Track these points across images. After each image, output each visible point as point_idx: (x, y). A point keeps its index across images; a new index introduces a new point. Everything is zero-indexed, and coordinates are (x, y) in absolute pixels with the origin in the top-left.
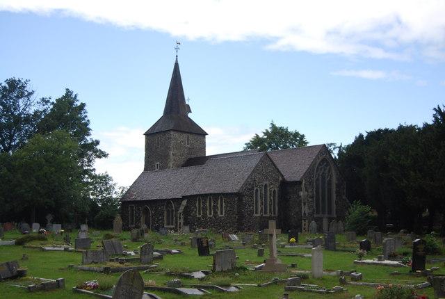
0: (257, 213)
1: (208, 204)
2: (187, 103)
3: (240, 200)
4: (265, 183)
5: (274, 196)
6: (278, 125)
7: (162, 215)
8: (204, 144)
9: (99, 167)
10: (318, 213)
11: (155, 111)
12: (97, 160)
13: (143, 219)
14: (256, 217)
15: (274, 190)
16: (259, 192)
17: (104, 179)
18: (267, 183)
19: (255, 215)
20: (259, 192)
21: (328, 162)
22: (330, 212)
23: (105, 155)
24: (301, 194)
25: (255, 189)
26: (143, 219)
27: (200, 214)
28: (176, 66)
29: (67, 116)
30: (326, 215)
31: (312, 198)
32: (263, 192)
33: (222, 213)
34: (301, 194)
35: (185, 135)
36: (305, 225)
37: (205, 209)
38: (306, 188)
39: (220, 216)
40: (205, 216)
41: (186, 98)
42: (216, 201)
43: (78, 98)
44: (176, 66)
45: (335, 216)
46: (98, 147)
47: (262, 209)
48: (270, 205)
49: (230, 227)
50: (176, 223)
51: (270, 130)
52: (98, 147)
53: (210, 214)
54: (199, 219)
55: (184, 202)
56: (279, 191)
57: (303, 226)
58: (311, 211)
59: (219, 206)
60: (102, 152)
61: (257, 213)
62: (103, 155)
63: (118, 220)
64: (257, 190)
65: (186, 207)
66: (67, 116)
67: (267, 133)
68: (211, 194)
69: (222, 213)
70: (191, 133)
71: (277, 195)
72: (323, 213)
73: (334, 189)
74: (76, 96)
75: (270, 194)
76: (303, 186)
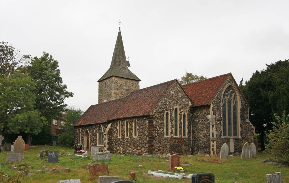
1: (125, 127)
3: (151, 122)
4: (175, 107)
7: (96, 136)
9: (70, 103)
10: (225, 135)
11: (105, 64)
14: (166, 139)
15: (184, 115)
16: (169, 115)
18: (178, 107)
19: (165, 136)
20: (169, 115)
21: (233, 89)
22: (235, 134)
23: (71, 95)
24: (209, 117)
25: (166, 112)
27: (120, 136)
28: (120, 34)
29: (45, 71)
31: (220, 120)
33: (136, 135)
34: (209, 117)
35: (124, 80)
36: (213, 146)
37: (123, 131)
38: (214, 111)
39: (134, 137)
44: (120, 34)
45: (240, 137)
47: (172, 131)
48: (180, 128)
49: (143, 147)
51: (185, 76)
54: (119, 139)
55: (109, 126)
56: (189, 115)
58: (219, 133)
59: (133, 128)
60: (67, 93)
61: (167, 134)
64: (167, 114)
65: (111, 130)
66: (45, 71)
67: (262, 72)
69: (136, 135)
70: (128, 79)
71: (186, 119)
72: (230, 134)
73: (239, 111)
74: (51, 56)
75: (181, 118)
76: (211, 110)
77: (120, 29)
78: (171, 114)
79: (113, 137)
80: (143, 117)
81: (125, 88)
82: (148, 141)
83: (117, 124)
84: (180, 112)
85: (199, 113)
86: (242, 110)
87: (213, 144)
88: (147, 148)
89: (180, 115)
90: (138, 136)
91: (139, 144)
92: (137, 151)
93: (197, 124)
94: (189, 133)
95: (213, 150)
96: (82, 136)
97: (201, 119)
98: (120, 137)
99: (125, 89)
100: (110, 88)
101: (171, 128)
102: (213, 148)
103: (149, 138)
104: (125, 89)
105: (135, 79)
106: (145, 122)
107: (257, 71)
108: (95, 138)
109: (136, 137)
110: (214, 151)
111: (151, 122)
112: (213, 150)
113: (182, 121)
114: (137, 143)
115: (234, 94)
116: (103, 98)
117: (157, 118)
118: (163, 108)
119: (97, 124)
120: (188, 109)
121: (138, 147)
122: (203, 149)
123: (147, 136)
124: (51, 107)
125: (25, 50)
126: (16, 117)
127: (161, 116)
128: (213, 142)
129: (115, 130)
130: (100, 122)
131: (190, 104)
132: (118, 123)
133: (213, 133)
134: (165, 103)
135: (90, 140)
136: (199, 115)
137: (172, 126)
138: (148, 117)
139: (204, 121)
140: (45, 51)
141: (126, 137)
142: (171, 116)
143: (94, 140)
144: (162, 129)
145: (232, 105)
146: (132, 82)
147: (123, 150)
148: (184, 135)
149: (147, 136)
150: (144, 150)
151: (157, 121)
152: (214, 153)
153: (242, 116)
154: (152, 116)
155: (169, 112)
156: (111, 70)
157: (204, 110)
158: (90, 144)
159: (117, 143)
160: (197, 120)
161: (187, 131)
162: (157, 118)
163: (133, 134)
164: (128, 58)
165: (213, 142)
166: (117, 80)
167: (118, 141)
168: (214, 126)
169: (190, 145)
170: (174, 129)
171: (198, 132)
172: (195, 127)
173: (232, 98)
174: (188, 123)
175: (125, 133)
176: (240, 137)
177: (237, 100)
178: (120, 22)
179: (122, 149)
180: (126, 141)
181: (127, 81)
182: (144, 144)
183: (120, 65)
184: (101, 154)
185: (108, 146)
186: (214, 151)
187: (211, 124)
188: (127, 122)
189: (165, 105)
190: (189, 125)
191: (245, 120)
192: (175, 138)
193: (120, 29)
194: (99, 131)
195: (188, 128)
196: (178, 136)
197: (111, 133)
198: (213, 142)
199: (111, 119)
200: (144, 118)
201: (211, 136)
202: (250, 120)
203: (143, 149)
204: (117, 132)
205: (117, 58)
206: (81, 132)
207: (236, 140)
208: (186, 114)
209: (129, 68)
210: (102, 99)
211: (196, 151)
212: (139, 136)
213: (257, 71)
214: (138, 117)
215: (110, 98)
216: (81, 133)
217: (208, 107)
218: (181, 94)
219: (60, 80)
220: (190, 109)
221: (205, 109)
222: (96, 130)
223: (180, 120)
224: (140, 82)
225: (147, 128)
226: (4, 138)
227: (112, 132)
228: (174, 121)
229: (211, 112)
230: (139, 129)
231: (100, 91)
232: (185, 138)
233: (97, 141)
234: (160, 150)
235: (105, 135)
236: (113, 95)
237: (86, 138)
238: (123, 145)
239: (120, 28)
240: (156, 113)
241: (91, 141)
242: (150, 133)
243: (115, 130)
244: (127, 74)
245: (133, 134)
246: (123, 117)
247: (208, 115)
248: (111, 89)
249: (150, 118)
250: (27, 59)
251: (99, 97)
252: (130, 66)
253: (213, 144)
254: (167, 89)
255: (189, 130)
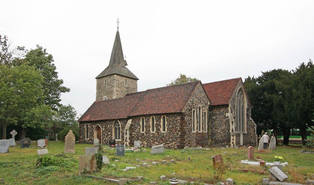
0: (194, 130)
2: (125, 59)
3: (182, 119)
5: (205, 116)
6: (183, 74)
8: (136, 85)
9: (65, 99)
11: (103, 63)
12: (62, 93)
13: (95, 134)
14: (193, 134)
15: (205, 112)
16: (195, 113)
17: (69, 109)
18: (201, 105)
19: (193, 132)
20: (195, 113)
23: (68, 90)
24: (228, 115)
26: (95, 134)
27: (143, 130)
29: (39, 60)
30: (242, 132)
32: (198, 113)
33: (164, 130)
34: (228, 115)
36: (233, 140)
39: (163, 132)
40: (148, 132)
41: (124, 56)
42: (158, 120)
43: (46, 52)
46: (62, 85)
47: (197, 127)
48: (203, 124)
50: (123, 137)
52: (62, 85)
53: (153, 130)
54: (143, 134)
55: (130, 122)
56: (208, 113)
57: (232, 141)
60: (64, 88)
61: (194, 130)
62: (65, 90)
63: (70, 135)
64: (194, 111)
65: (131, 125)
68: (154, 115)
69: (164, 130)
70: (128, 77)
74: (45, 50)
75: (203, 115)
76: (229, 109)
77: (118, 29)
78: (197, 112)
79: (134, 132)
80: (173, 114)
81: (125, 86)
82: (180, 135)
83: (140, 120)
84: (203, 110)
85: (216, 111)
86: (248, 110)
87: (233, 138)
88: (179, 142)
89: (203, 112)
90: (168, 131)
91: (169, 138)
92: (166, 145)
93: (214, 121)
94: (208, 128)
95: (233, 143)
96: (91, 131)
97: (219, 116)
98: (144, 132)
99: (125, 87)
100: (112, 85)
101: (197, 125)
102: (233, 141)
103: (181, 133)
104: (125, 87)
105: (133, 77)
106: (176, 118)
107: (249, 77)
108: (109, 133)
109: (165, 132)
110: (234, 145)
111: (182, 119)
112: (233, 143)
113: (204, 118)
114: (166, 137)
115: (242, 96)
116: (102, 94)
117: (188, 115)
118: (191, 106)
119: (114, 120)
120: (207, 107)
121: (167, 141)
122: (221, 142)
123: (179, 131)
124: (2, 103)
125: (21, 42)
126: (32, 112)
127: (190, 113)
128: (233, 136)
129: (136, 126)
130: (117, 118)
131: (209, 103)
132: (141, 119)
133: (233, 129)
134: (193, 101)
135: (103, 135)
136: (216, 113)
137: (197, 122)
138: (180, 114)
139: (223, 118)
140: (38, 44)
141: (151, 132)
142: (197, 113)
143: (108, 135)
144: (191, 125)
145: (241, 105)
146: (131, 81)
147: (147, 144)
148: (205, 131)
149: (179, 131)
150: (175, 144)
151: (188, 117)
152: (234, 146)
153: (247, 115)
154: (184, 113)
155: (195, 110)
156: (111, 67)
157: (222, 109)
158: (103, 139)
159: (139, 138)
160: (215, 118)
161: (207, 127)
162: (188, 115)
163: (161, 129)
164: (125, 57)
165: (233, 136)
166: (119, 77)
167: (141, 136)
168: (234, 123)
169: (213, 139)
170: (198, 125)
171: (215, 128)
172: (213, 123)
173: (241, 99)
174: (208, 120)
175: (151, 129)
176: (246, 132)
177: (244, 101)
178: (118, 22)
179: (146, 143)
180: (151, 135)
181: (127, 79)
182: (175, 138)
183: (119, 64)
184: (157, 148)
185: (129, 140)
186: (234, 145)
187: (231, 120)
188: (153, 118)
189: (192, 103)
190: (208, 122)
191: (249, 118)
192: (199, 133)
193: (118, 29)
194: (114, 126)
195: (207, 125)
196: (201, 132)
197: (132, 128)
198: (233, 137)
199: (132, 115)
200: (175, 115)
201: (231, 131)
202: (252, 118)
203: (173, 143)
204: (139, 127)
205: (116, 56)
206: (89, 127)
207: (244, 134)
208: (206, 111)
209: (126, 66)
210: (101, 96)
211: (213, 144)
212: (169, 132)
213: (249, 77)
214: (168, 114)
215: (112, 95)
216: (90, 128)
217: (227, 106)
218: (203, 94)
219: (55, 74)
220: (209, 108)
221: (223, 108)
222: (112, 126)
223: (202, 117)
224: (138, 81)
225: (179, 124)
226: (17, 133)
227: (133, 127)
228: (198, 118)
229: (229, 111)
230: (168, 125)
231: (99, 87)
232: (205, 133)
233: (112, 135)
234: (189, 143)
235: (127, 130)
236: (115, 92)
237: (96, 133)
238: (148, 140)
239: (118, 27)
240: (186, 110)
241: (104, 136)
242: (182, 129)
243: (136, 126)
244: (127, 72)
245: (161, 129)
246: (150, 113)
247: (226, 114)
248: (113, 87)
249: (182, 115)
250: (21, 51)
251: (97, 93)
252: (127, 65)
253: (233, 138)
254: (193, 89)
255: (208, 126)
